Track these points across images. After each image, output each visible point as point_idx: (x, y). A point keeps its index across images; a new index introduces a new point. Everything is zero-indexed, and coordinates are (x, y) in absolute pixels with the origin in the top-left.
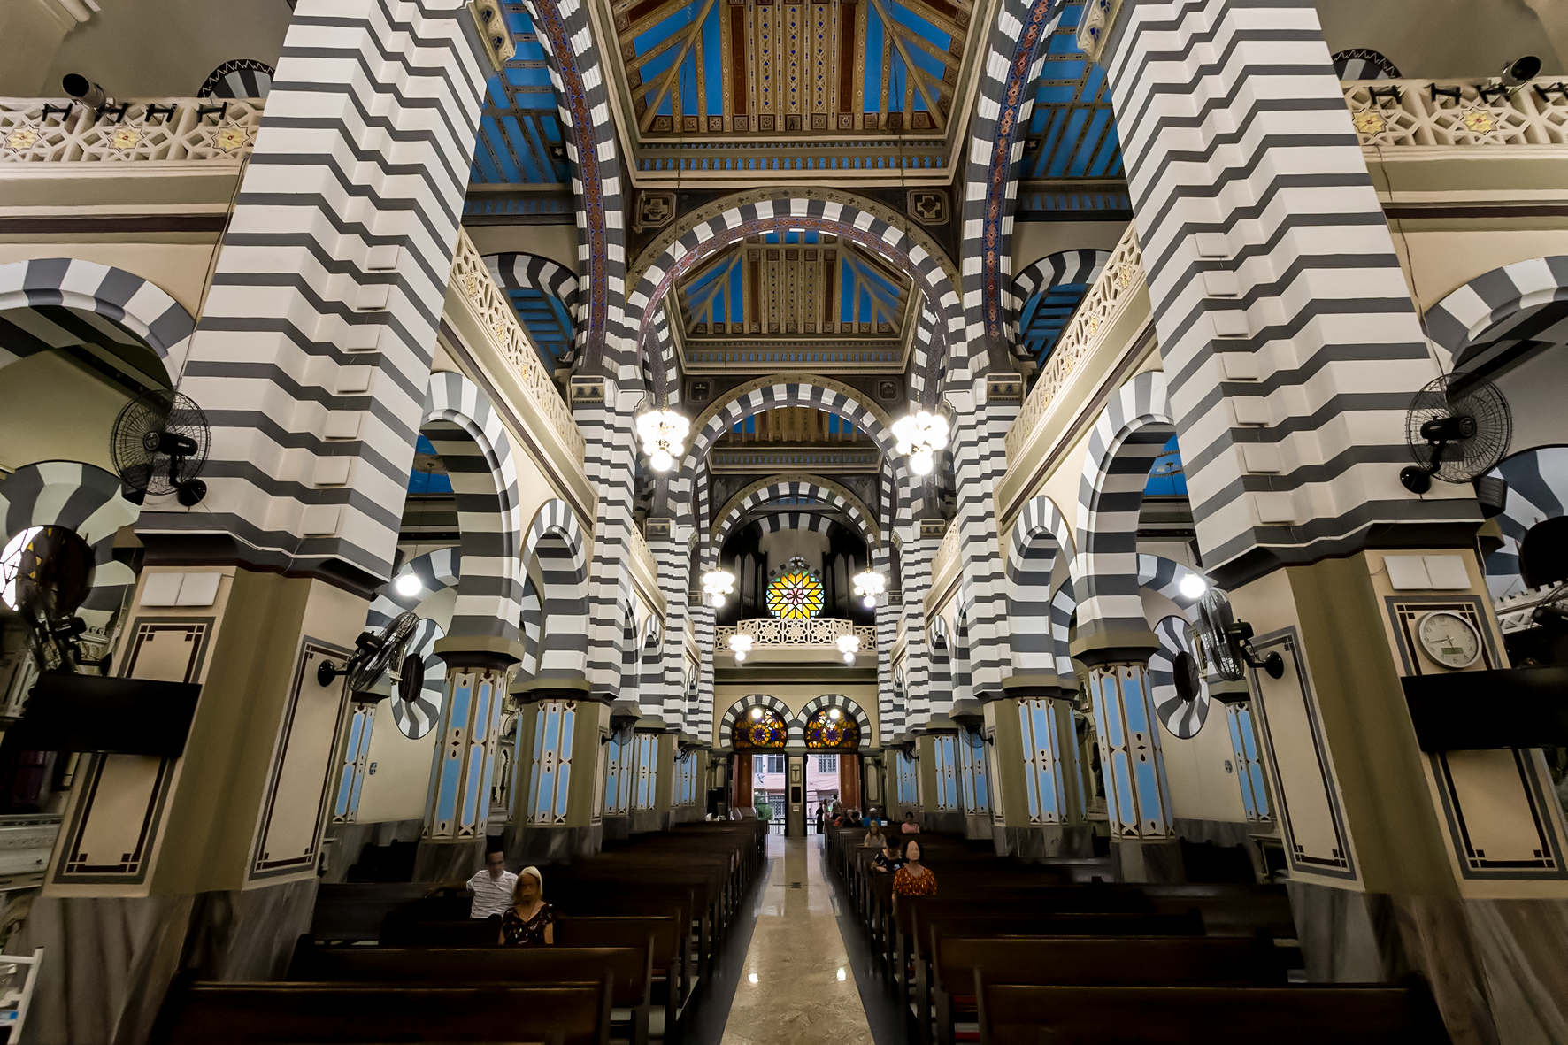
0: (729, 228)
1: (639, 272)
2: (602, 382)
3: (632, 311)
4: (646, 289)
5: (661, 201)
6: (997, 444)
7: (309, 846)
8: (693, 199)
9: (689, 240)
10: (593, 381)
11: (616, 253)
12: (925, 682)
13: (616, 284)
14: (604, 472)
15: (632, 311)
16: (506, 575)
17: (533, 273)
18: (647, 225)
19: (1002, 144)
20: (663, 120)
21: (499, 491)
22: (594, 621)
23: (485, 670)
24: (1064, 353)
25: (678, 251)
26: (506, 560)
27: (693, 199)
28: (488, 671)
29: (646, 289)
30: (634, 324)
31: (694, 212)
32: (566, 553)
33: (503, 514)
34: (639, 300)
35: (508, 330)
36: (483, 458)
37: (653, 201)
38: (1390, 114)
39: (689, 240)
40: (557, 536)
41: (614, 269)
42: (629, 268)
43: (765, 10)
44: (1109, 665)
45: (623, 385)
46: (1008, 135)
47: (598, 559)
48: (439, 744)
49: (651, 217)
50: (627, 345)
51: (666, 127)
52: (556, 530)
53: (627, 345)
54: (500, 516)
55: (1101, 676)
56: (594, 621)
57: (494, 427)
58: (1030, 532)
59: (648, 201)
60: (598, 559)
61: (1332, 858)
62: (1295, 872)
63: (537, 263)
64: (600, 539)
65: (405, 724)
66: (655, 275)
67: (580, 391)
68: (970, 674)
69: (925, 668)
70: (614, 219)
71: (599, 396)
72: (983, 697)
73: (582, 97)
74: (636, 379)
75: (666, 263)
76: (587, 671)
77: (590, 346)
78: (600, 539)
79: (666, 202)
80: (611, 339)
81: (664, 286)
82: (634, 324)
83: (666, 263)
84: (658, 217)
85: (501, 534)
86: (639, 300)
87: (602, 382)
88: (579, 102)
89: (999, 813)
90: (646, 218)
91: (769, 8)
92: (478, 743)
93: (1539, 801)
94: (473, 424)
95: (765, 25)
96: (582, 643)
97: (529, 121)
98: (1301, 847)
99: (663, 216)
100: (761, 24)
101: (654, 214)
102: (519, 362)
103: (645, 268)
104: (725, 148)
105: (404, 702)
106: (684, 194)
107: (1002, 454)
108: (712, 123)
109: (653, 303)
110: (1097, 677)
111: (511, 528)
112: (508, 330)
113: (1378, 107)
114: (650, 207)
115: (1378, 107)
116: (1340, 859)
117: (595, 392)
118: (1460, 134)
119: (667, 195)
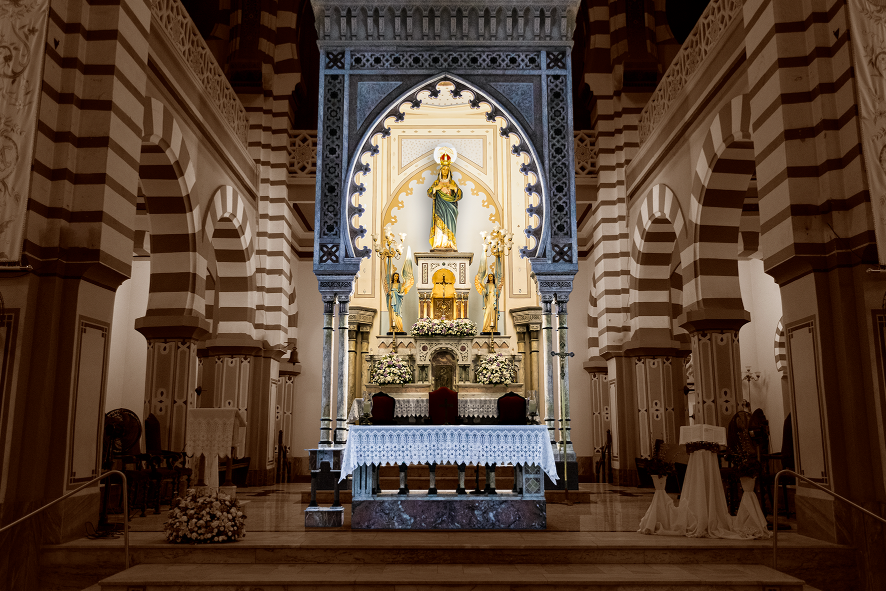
6: (632, 119)
7: (792, 340)
12: (625, 291)
14: (263, 154)
24: (711, 17)
28: (184, 340)
40: (228, 220)
44: (706, 332)
48: (147, 402)
52: (227, 215)
55: (699, 340)
58: (651, 215)
61: (87, 328)
62: (800, 487)
68: (597, 339)
69: (626, 272)
72: (606, 356)
73: (357, 107)
74: (293, 59)
89: (615, 455)
93: (8, 374)
98: (103, 336)
102: (225, 106)
107: (634, 128)
110: (697, 341)
112: (182, 24)
116: (824, 477)
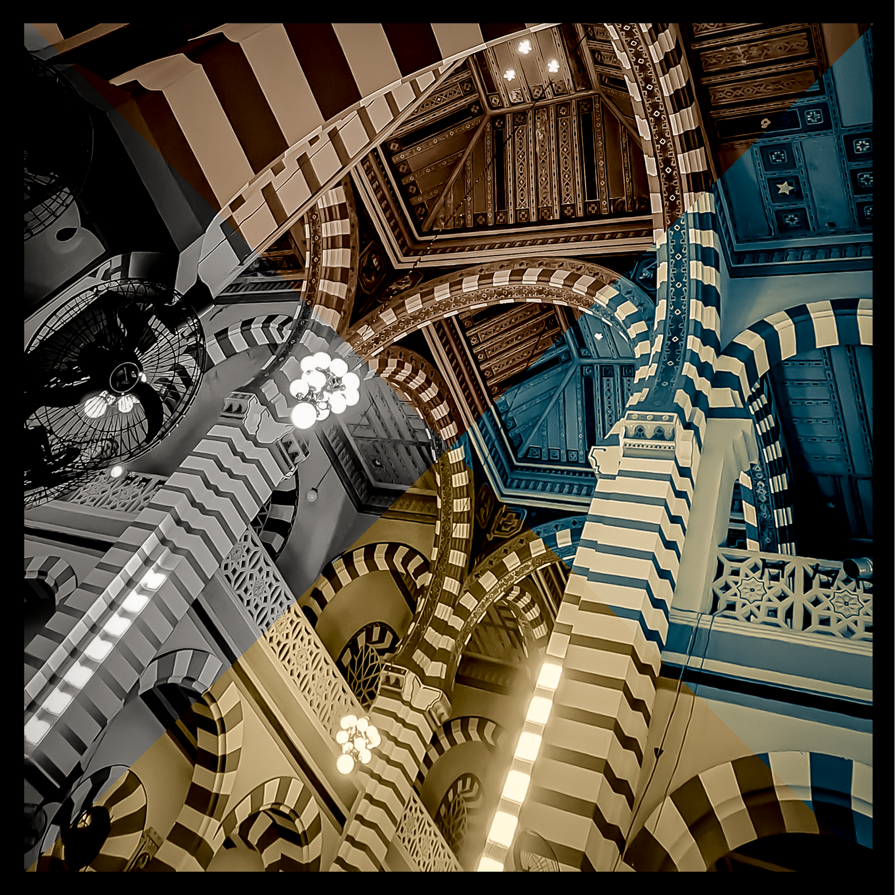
1: (477, 576)
3: (460, 611)
5: (514, 515)
9: (524, 553)
10: (398, 671)
11: (457, 558)
13: (451, 585)
15: (460, 611)
18: (498, 535)
19: (764, 509)
21: (220, 754)
25: (512, 561)
26: (206, 818)
30: (457, 623)
31: (553, 522)
33: (218, 774)
36: (214, 722)
38: (771, 585)
41: (452, 571)
43: (608, 380)
45: (426, 680)
46: (767, 502)
50: (445, 643)
51: (537, 455)
53: (445, 643)
59: (504, 515)
64: (350, 839)
66: (488, 581)
70: (461, 531)
71: (401, 688)
75: (500, 571)
77: (413, 637)
78: (350, 839)
79: (518, 516)
80: (431, 635)
81: (496, 591)
83: (500, 571)
84: (508, 529)
85: (210, 793)
86: (469, 602)
94: (209, 694)
95: (609, 390)
99: (512, 528)
101: (506, 526)
104: (583, 477)
109: (484, 606)
111: (220, 791)
114: (505, 519)
117: (397, 683)
118: (827, 614)
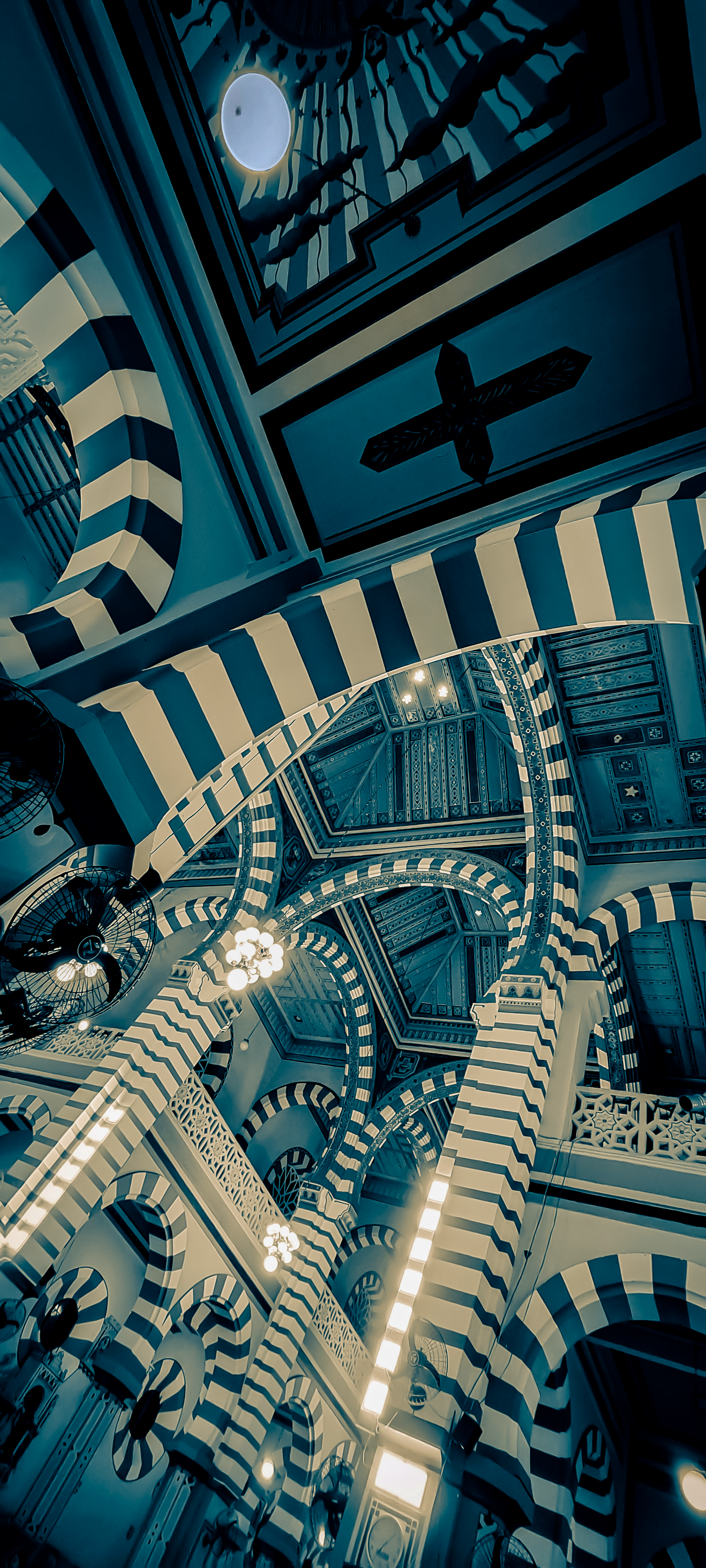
0: (425, 1093)
2: (319, 1190)
4: (380, 1123)
5: (409, 1059)
8: (430, 1061)
9: (417, 1091)
10: (314, 1187)
11: (363, 1095)
13: (357, 1117)
15: (365, 1138)
16: (151, 1321)
17: (320, 1098)
18: (396, 1076)
20: (426, 1006)
21: (168, 1255)
22: (242, 1404)
23: (107, 1391)
25: (407, 1097)
26: (157, 1308)
27: (430, 1061)
29: (380, 1123)
30: (363, 1148)
32: (232, 1326)
34: (372, 1130)
35: (227, 1147)
37: (405, 1059)
39: (417, 1091)
42: (371, 1109)
45: (338, 1195)
47: (267, 1344)
49: (400, 1071)
50: (353, 1164)
53: (353, 1164)
54: (164, 1274)
55: (184, 1483)
56: (242, 1404)
57: (177, 1210)
59: (401, 1059)
60: (267, 1344)
63: (326, 1090)
64: (275, 1325)
65: (119, 1457)
66: (388, 1113)
67: (306, 1193)
71: (316, 1201)
75: (398, 1105)
76: (217, 1452)
78: (275, 1325)
79: (412, 1061)
82: (363, 1148)
84: (404, 1071)
85: (160, 1287)
86: (372, 1130)
87: (319, 1190)
88: (350, 1004)
90: (397, 1071)
91: (489, 948)
92: (75, 1451)
96: (224, 1421)
97: (336, 1006)
100: (484, 956)
101: (403, 1068)
103: (383, 1107)
105: (129, 1434)
106: (425, 1057)
108: (455, 1010)
109: (384, 1133)
113: (693, 1122)
114: (402, 1063)
115: (693, 1122)
117: (314, 1197)
119: (414, 1056)
